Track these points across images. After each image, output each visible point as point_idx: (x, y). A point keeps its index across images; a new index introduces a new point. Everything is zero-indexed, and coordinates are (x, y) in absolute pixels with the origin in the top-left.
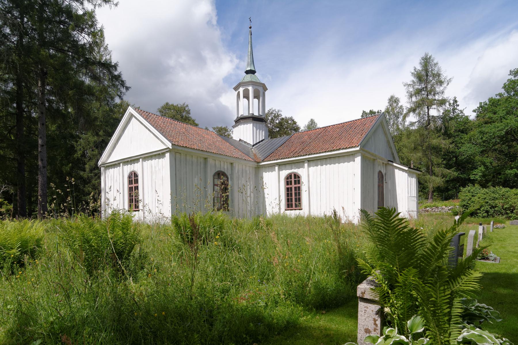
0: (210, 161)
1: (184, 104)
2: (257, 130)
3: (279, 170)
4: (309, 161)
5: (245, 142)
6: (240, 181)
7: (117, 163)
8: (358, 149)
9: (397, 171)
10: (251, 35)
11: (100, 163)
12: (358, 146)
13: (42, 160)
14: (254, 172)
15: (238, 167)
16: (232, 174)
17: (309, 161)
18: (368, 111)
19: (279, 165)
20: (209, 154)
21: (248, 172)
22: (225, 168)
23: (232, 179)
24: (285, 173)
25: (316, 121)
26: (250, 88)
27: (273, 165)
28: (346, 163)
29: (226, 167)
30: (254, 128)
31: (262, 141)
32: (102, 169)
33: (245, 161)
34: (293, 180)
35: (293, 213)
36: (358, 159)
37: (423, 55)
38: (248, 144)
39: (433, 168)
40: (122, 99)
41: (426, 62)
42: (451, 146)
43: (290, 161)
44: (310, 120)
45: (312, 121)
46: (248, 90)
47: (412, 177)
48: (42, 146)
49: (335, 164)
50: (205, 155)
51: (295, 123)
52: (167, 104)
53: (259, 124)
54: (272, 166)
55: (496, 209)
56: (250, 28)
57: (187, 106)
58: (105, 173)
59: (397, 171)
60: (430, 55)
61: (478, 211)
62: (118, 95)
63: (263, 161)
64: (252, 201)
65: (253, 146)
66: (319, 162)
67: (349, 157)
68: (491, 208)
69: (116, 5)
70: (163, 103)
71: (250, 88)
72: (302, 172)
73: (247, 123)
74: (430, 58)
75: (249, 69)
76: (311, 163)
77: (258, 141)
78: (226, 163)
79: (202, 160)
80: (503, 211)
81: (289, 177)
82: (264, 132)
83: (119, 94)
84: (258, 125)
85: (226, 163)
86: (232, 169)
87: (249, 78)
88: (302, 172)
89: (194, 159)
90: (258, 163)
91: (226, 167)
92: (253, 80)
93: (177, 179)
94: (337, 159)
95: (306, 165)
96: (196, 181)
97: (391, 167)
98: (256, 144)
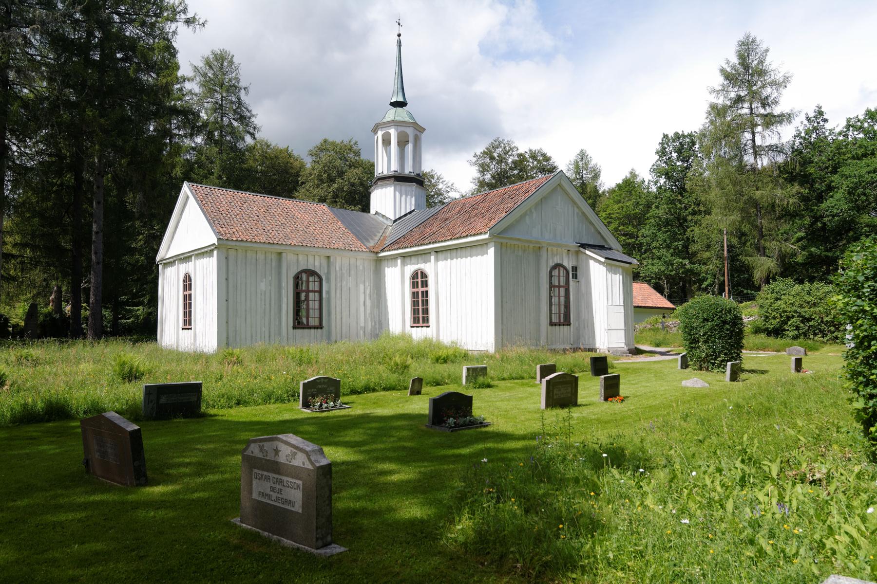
0: (289, 257)
1: (350, 142)
2: (401, 196)
3: (404, 264)
4: (437, 251)
5: (383, 216)
6: (344, 283)
7: (172, 260)
8: (487, 236)
9: (591, 262)
10: (400, 46)
11: (158, 258)
12: (486, 233)
13: (96, 253)
14: (373, 268)
15: (340, 262)
16: (329, 273)
17: (437, 251)
18: (671, 134)
19: (404, 256)
20: (283, 247)
21: (361, 268)
22: (316, 263)
23: (328, 280)
24: (410, 269)
25: (590, 153)
26: (393, 132)
27: (394, 258)
28: (479, 257)
29: (317, 263)
30: (397, 194)
31: (410, 213)
32: (160, 267)
33: (351, 253)
34: (419, 280)
35: (418, 334)
36: (491, 251)
37: (741, 37)
38: (387, 218)
39: (762, 242)
40: (254, 138)
41: (746, 49)
42: (791, 201)
43: (477, 241)
44: (579, 152)
45: (583, 155)
46: (389, 134)
47: (616, 274)
48: (97, 233)
49: (466, 257)
50: (278, 249)
51: (547, 159)
52: (325, 141)
53: (405, 186)
54: (394, 258)
55: (811, 323)
56: (399, 35)
57: (355, 143)
58: (164, 273)
59: (591, 262)
60: (753, 35)
61: (786, 327)
62: (249, 133)
63: (383, 250)
64: (368, 311)
65: (395, 221)
66: (448, 254)
67: (478, 247)
68: (802, 322)
69: (203, 25)
70: (318, 141)
71: (393, 132)
72: (428, 267)
73: (386, 186)
74: (753, 41)
75: (394, 100)
76: (440, 255)
77: (403, 214)
78: (317, 258)
79: (274, 257)
80: (823, 326)
81: (415, 276)
82: (413, 199)
83: (251, 130)
84: (403, 188)
85: (317, 258)
86: (329, 266)
87: (392, 114)
88: (428, 267)
89: (261, 256)
90: (377, 253)
91: (317, 263)
92: (398, 118)
93: (231, 285)
94: (469, 249)
95: (433, 258)
96: (263, 286)
97: (585, 256)
98: (400, 218)
